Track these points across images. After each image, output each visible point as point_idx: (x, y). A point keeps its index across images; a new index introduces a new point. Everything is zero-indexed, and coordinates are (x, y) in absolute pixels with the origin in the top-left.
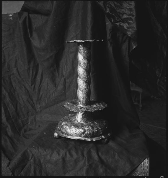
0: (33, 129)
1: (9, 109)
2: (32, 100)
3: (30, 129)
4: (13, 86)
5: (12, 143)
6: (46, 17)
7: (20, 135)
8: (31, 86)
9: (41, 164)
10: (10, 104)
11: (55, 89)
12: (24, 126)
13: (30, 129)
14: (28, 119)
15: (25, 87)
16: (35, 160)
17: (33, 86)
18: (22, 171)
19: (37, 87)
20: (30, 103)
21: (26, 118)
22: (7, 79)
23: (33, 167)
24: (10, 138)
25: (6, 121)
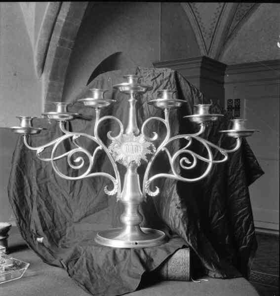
0: (117, 193)
1: (45, 219)
2: (70, 209)
3: (68, 240)
4: (49, 194)
5: (51, 252)
6: (88, 122)
7: (58, 247)
8: (70, 193)
9: (92, 257)
10: (47, 213)
11: (96, 195)
12: (61, 237)
13: (68, 240)
14: (65, 230)
15: (63, 195)
16: (86, 256)
17: (71, 194)
18: (75, 263)
19: (76, 195)
20: (68, 212)
21: (63, 229)
22: (43, 185)
23: (85, 260)
24: (48, 249)
25: (42, 231)
